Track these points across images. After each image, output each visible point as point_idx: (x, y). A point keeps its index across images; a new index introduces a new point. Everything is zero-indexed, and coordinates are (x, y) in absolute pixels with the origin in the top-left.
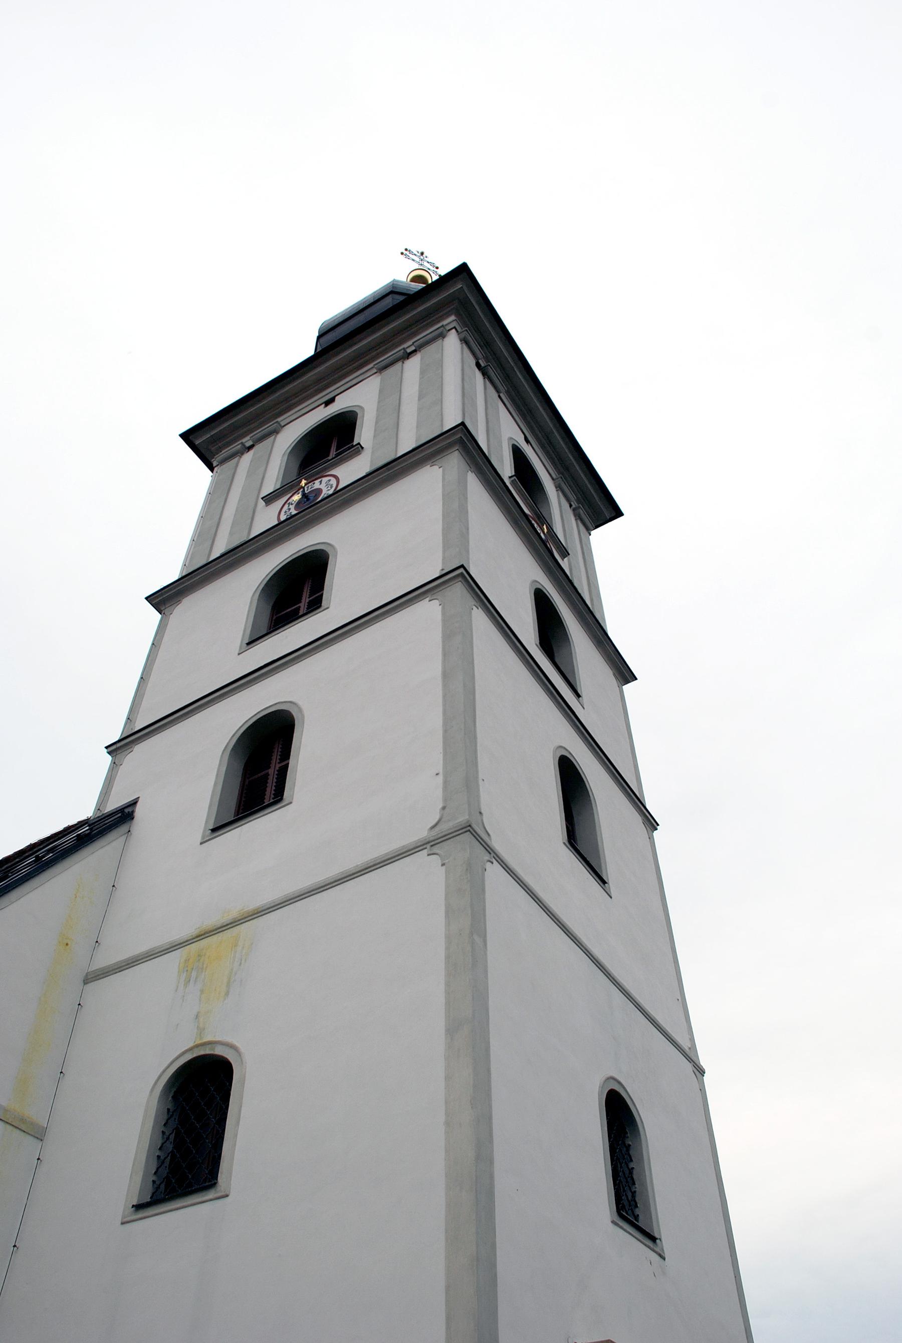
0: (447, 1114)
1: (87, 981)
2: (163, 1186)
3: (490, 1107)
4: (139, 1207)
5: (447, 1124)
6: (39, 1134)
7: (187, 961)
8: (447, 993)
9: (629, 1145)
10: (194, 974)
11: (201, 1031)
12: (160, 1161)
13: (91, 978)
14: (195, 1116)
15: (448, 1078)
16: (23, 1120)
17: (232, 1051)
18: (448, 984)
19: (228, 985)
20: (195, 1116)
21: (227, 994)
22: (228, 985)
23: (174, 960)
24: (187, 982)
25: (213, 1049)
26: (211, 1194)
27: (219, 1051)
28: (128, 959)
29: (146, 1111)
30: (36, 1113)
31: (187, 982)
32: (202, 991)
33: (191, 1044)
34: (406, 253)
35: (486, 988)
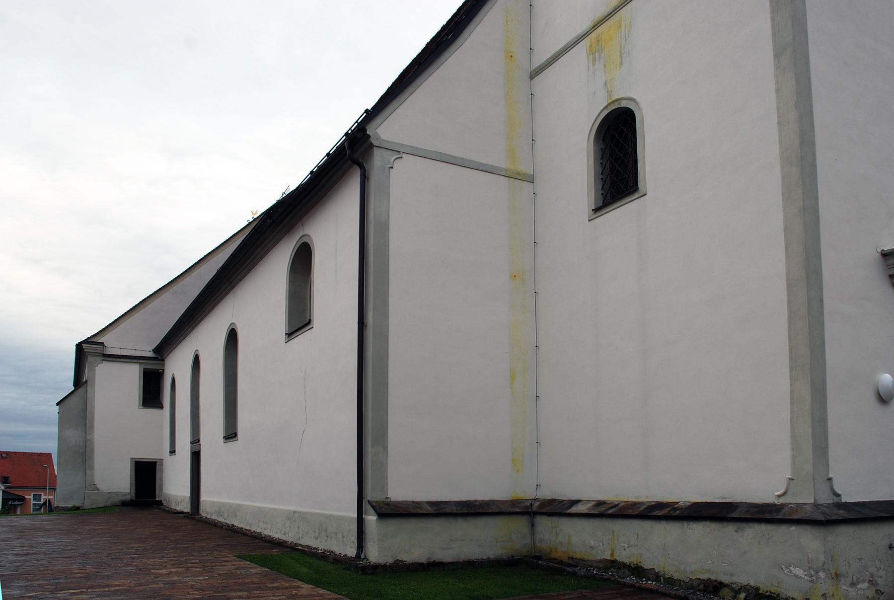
0: (779, 117)
1: (532, 77)
2: (609, 195)
3: (811, 106)
4: (596, 210)
5: (779, 123)
6: (530, 179)
7: (591, 46)
8: (773, 27)
9: (15, 512)
10: (597, 55)
11: (610, 93)
12: (604, 181)
13: (535, 74)
14: (618, 148)
15: (777, 91)
16: (518, 173)
17: (632, 102)
18: (773, 19)
19: (621, 57)
20: (618, 148)
21: (621, 63)
22: (621, 57)
23: (583, 46)
24: (594, 61)
25: (620, 104)
26: (636, 195)
27: (624, 104)
28: (552, 56)
29: (588, 153)
30: (524, 167)
31: (594, 61)
32: (605, 66)
33: (606, 104)
34: (86, 382)
35: (805, 15)
